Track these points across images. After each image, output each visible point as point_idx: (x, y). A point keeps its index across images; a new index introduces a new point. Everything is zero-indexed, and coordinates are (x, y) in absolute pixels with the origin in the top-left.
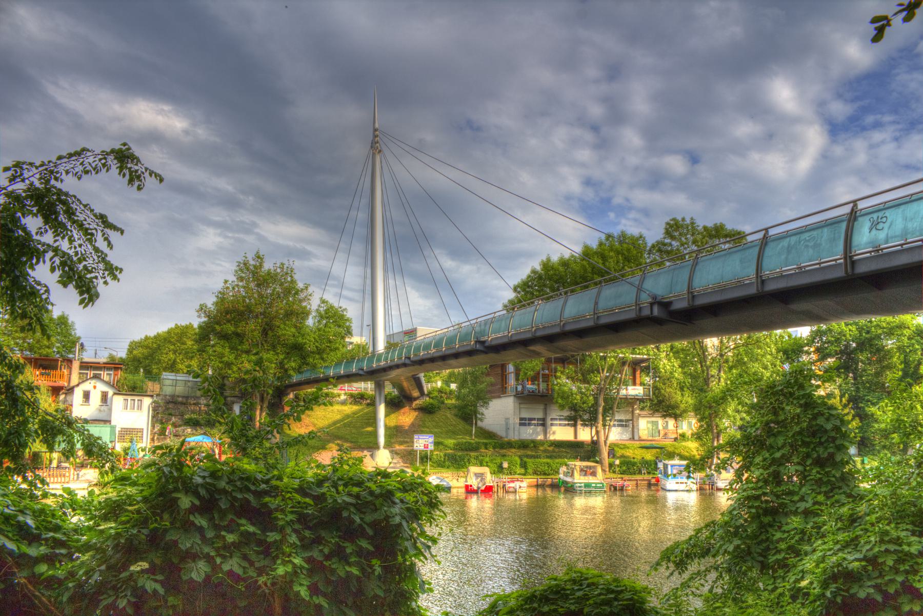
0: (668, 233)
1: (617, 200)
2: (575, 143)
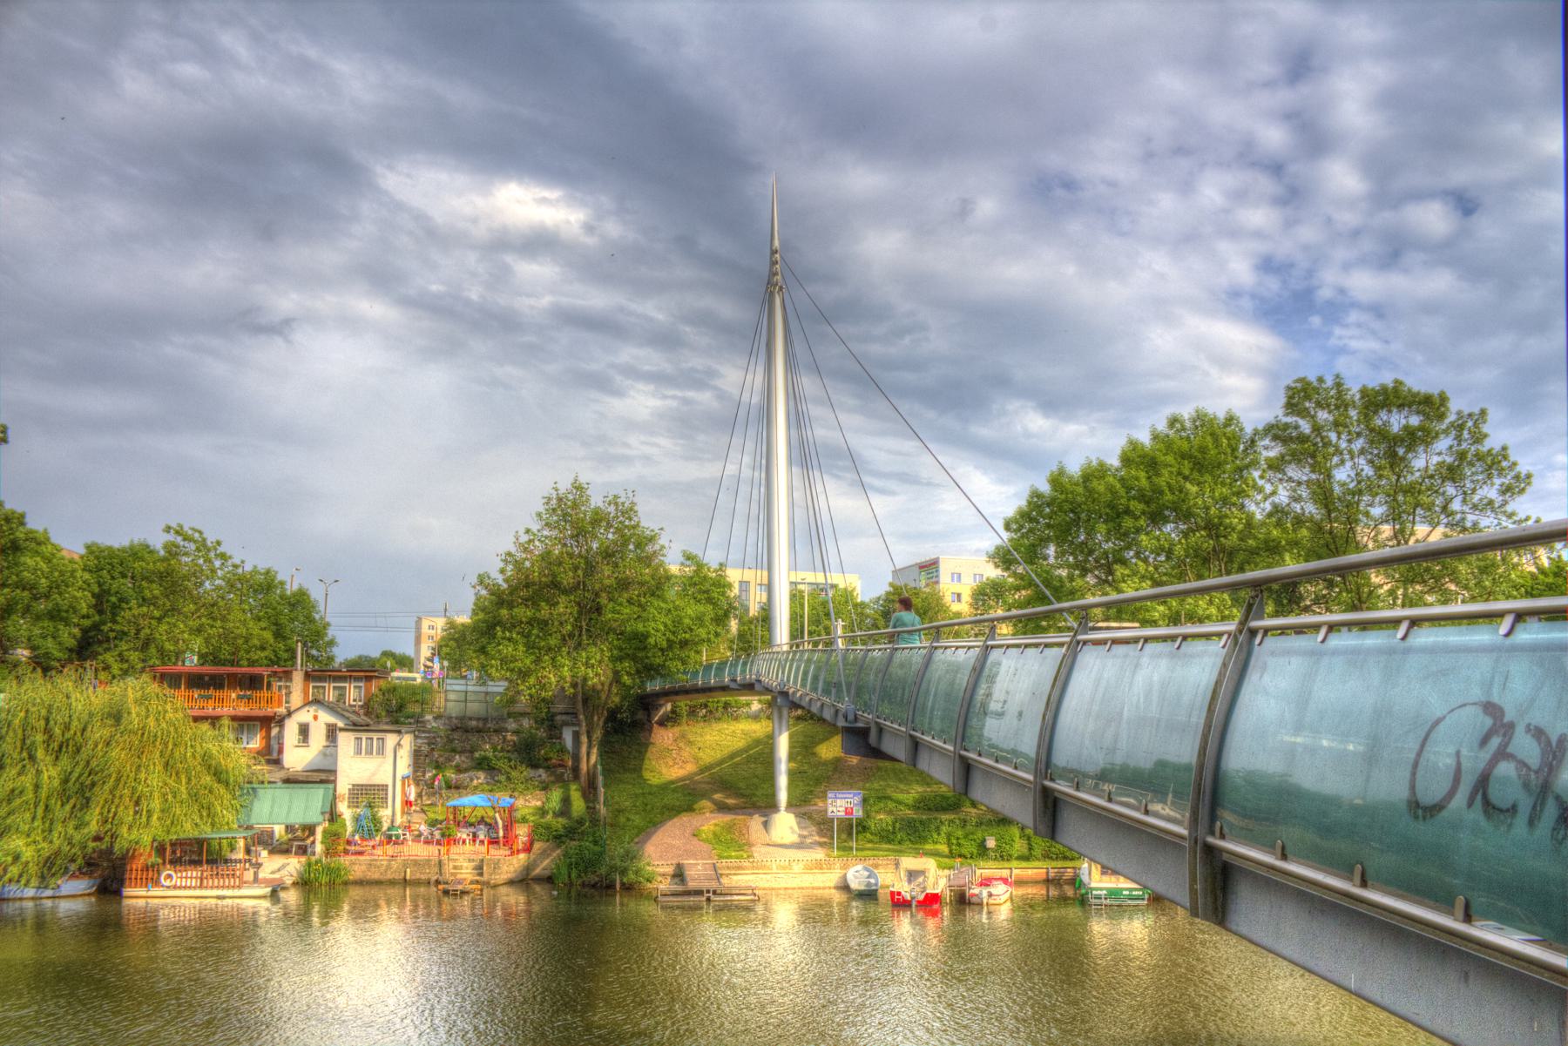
0: (1292, 406)
1: (1325, 293)
2: (1240, 196)
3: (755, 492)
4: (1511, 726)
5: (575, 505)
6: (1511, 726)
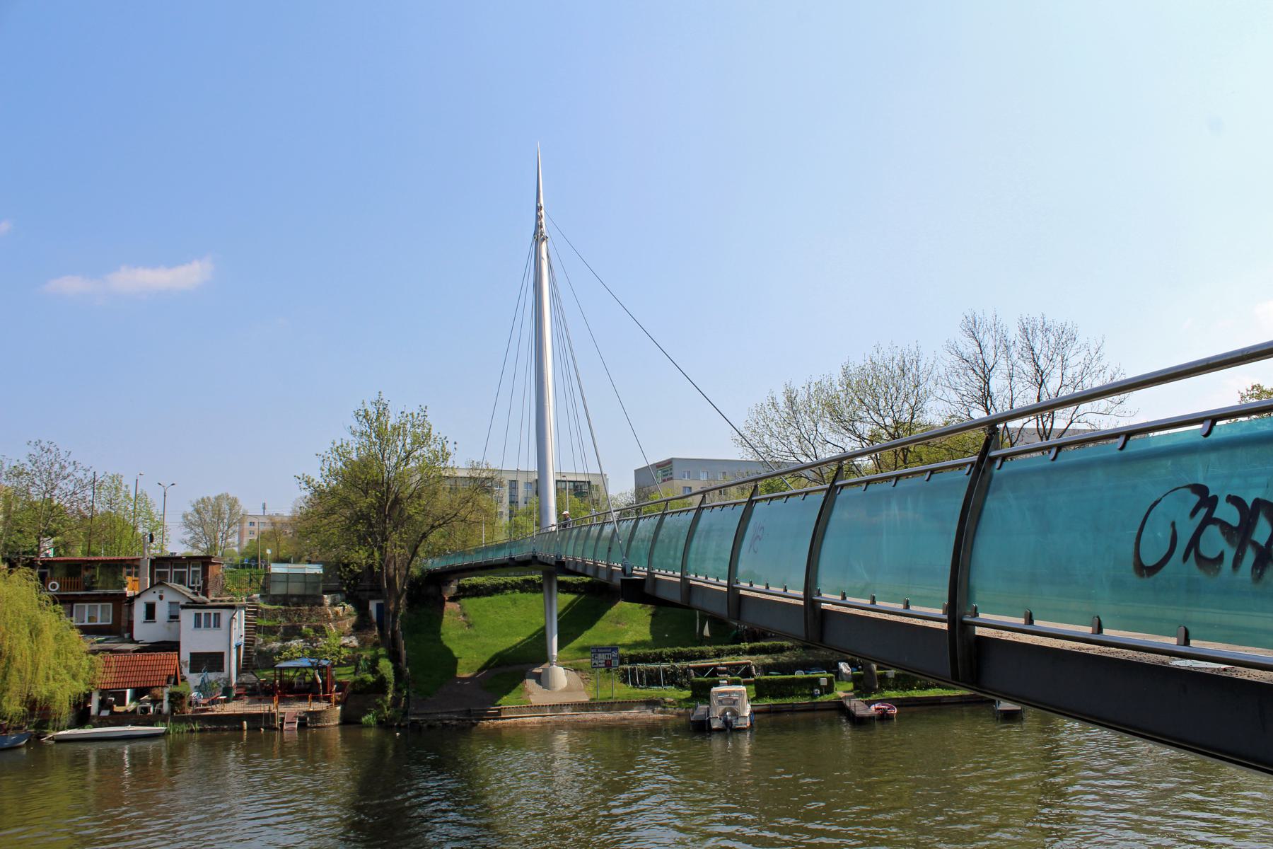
3: (271, 821)
4: (1215, 499)
6: (1215, 499)
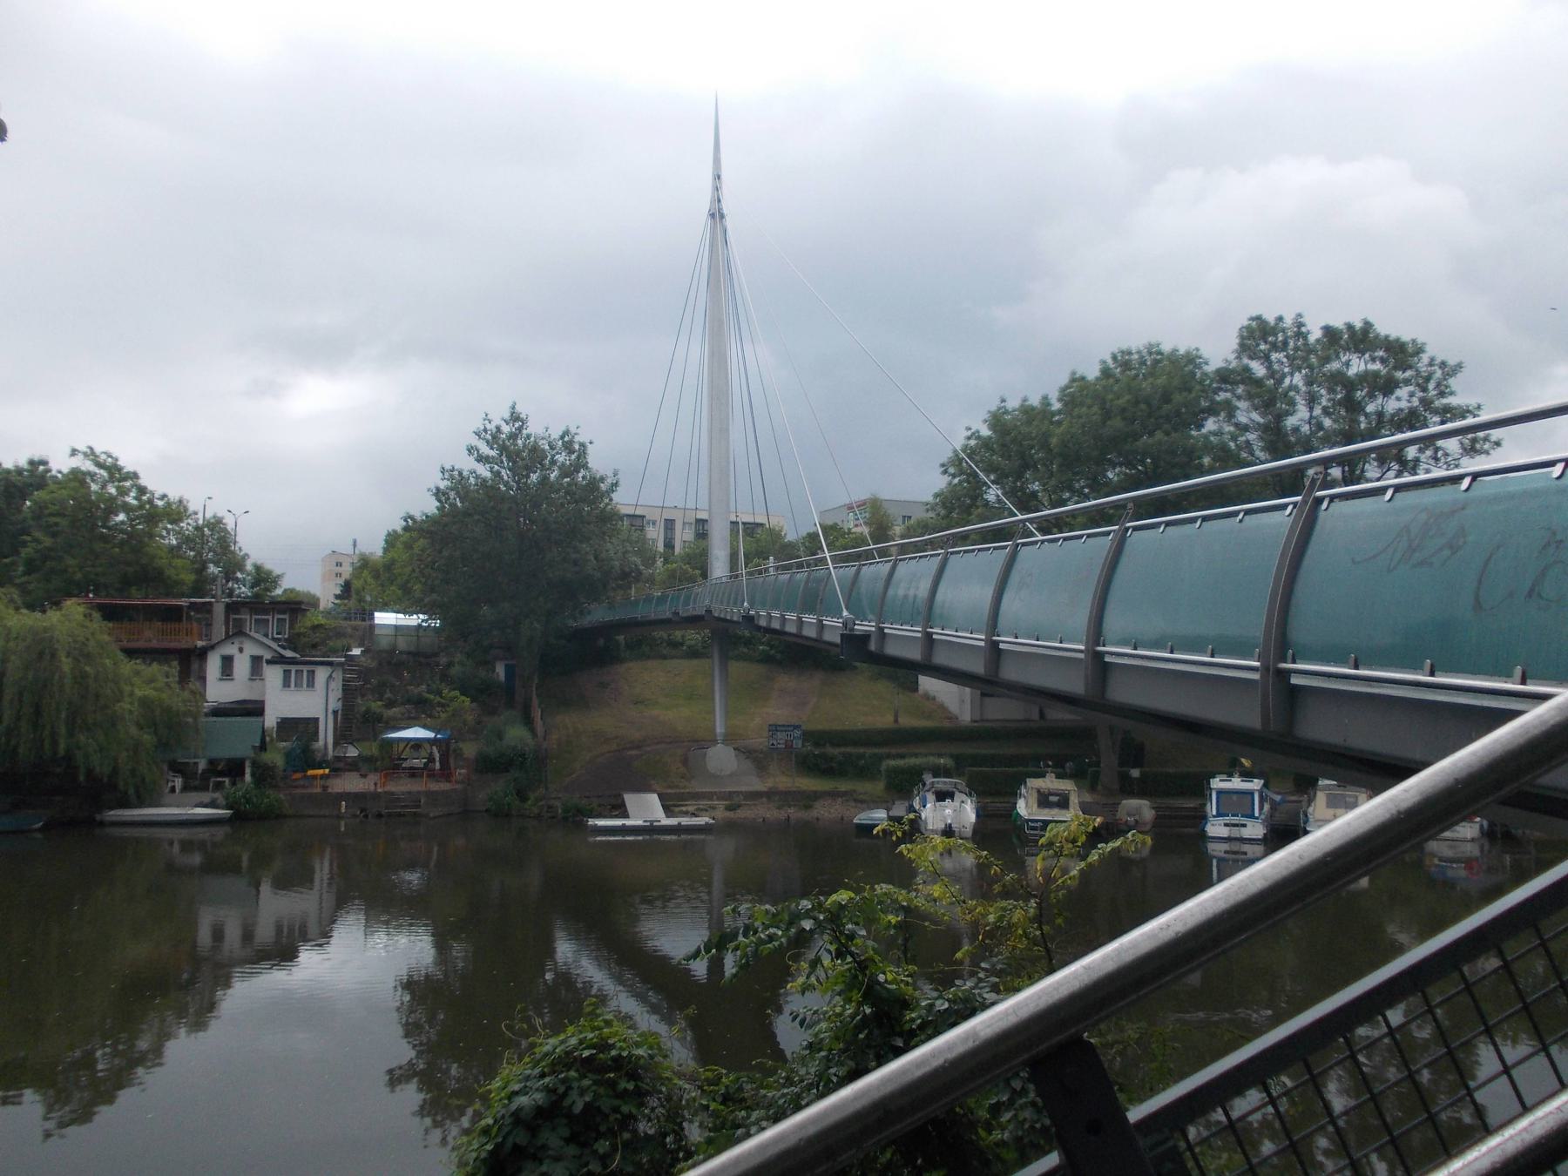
5: (513, 436)
